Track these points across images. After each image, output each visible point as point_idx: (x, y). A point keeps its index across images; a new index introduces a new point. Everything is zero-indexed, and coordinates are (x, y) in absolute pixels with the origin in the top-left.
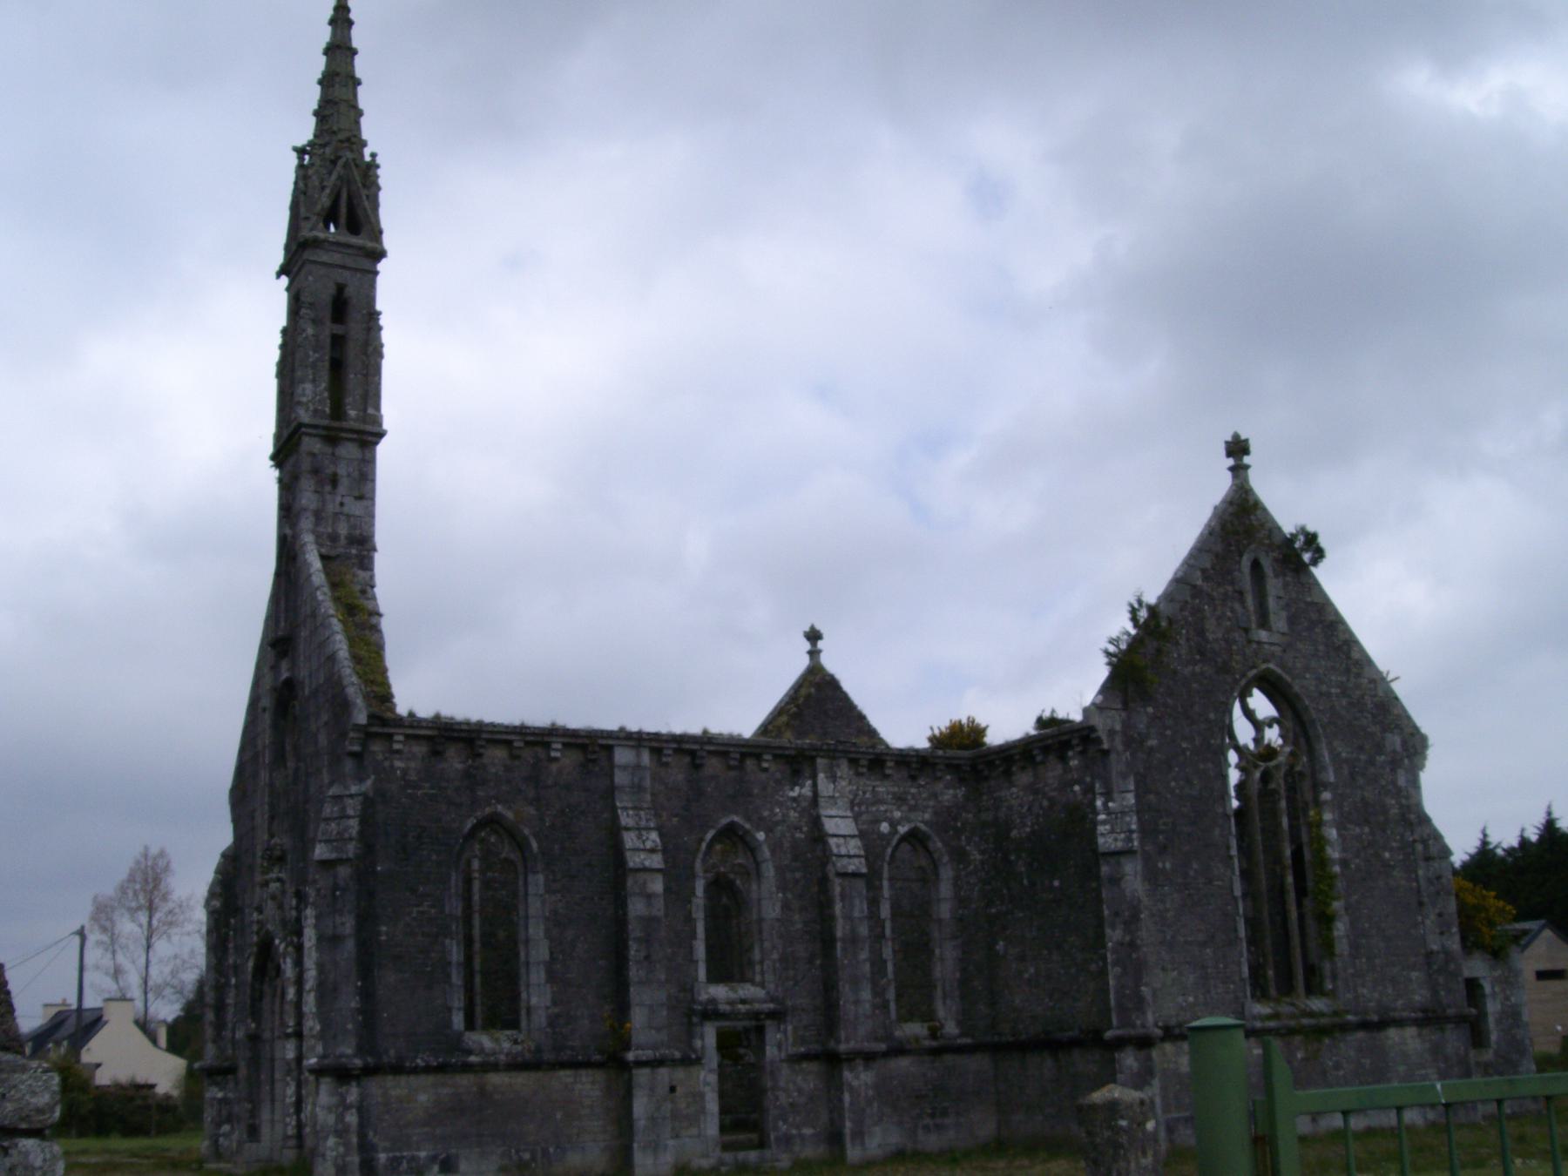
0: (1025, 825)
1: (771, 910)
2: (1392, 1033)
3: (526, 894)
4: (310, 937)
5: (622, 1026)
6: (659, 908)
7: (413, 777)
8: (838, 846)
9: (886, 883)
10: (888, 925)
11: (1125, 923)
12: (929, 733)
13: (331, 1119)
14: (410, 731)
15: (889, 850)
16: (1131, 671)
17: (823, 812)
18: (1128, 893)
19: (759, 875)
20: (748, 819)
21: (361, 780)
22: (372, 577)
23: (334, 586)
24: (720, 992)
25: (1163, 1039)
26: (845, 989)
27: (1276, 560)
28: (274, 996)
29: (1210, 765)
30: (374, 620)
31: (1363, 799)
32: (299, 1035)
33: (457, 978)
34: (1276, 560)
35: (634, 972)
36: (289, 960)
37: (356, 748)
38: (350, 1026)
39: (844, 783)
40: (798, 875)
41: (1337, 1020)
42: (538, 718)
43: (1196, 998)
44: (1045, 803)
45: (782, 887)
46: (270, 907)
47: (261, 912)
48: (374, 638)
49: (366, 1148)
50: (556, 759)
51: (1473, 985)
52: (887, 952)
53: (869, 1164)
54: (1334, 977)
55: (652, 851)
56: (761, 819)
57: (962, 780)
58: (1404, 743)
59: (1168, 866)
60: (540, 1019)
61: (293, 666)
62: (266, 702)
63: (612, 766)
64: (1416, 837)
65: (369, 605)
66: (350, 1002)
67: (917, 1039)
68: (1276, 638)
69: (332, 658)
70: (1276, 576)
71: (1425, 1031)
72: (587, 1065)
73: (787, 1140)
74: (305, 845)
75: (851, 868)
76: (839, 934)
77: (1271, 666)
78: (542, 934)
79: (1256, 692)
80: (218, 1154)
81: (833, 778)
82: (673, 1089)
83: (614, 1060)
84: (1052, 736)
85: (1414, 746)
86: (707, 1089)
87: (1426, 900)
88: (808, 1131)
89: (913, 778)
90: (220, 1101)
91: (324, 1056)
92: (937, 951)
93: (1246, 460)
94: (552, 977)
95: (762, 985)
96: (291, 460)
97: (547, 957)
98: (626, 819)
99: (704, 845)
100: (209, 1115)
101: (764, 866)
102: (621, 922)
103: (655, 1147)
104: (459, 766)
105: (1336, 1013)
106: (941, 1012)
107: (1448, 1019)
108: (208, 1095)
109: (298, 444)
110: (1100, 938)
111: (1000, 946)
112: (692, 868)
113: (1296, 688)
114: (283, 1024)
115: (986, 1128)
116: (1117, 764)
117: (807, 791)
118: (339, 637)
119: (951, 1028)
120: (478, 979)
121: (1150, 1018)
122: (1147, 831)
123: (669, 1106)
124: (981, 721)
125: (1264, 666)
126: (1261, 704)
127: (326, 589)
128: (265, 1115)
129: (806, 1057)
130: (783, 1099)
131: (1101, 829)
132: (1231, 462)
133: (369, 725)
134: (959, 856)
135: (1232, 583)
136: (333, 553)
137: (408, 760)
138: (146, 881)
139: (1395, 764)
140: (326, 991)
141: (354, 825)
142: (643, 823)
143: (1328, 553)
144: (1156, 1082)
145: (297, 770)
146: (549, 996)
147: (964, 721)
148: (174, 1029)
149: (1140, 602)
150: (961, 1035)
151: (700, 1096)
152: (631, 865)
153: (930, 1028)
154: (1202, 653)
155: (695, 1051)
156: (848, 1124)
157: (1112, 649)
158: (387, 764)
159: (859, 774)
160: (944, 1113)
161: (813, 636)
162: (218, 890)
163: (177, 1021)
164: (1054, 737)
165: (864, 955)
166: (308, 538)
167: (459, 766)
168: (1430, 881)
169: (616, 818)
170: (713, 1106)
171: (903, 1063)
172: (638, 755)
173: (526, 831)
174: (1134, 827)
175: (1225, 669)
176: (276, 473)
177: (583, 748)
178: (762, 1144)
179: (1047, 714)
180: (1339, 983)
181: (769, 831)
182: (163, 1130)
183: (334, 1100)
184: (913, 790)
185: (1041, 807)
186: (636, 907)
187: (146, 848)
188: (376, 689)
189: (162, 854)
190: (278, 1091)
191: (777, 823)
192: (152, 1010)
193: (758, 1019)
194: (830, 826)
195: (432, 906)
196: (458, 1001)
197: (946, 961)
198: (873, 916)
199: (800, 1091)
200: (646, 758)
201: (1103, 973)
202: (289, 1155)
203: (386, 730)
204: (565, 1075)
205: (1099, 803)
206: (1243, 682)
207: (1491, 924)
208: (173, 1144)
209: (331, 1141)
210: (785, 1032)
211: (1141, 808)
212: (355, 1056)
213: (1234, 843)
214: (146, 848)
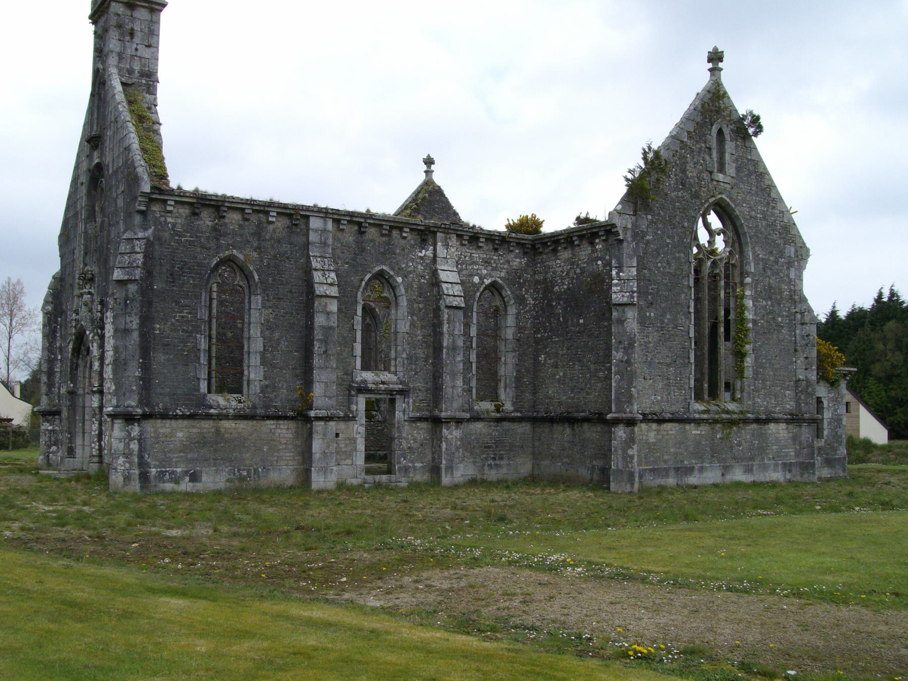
0: (564, 284)
1: (403, 327)
2: (772, 426)
3: (250, 308)
4: (109, 330)
5: (308, 394)
6: (334, 321)
7: (179, 228)
8: (448, 289)
9: (475, 314)
10: (474, 340)
11: (624, 348)
12: (507, 223)
13: (121, 446)
14: (178, 199)
15: (478, 294)
16: (639, 193)
17: (439, 267)
18: (628, 330)
19: (397, 304)
20: (393, 269)
21: (146, 229)
22: (155, 99)
23: (130, 103)
24: (369, 376)
25: (641, 421)
26: (447, 378)
27: (732, 130)
28: (85, 366)
29: (682, 255)
30: (156, 127)
31: (769, 284)
32: (101, 392)
33: (203, 360)
34: (732, 130)
35: (316, 361)
36: (95, 344)
37: (143, 208)
38: (134, 388)
39: (453, 250)
40: (421, 306)
41: (742, 416)
42: (262, 196)
43: (662, 397)
44: (578, 271)
45: (412, 313)
46: (84, 311)
47: (78, 314)
48: (156, 138)
49: (142, 464)
50: (272, 222)
51: (819, 401)
52: (473, 357)
53: (456, 487)
54: (742, 391)
55: (331, 284)
56: (400, 269)
57: (525, 253)
58: (796, 251)
59: (652, 315)
60: (256, 388)
61: (102, 155)
62: (84, 179)
63: (308, 229)
64: (797, 310)
65: (153, 117)
66: (134, 371)
67: (488, 412)
68: (728, 180)
69: (128, 149)
70: (731, 141)
71: (790, 427)
72: (285, 418)
73: (406, 470)
74: (107, 270)
75: (455, 304)
76: (445, 345)
77: (724, 196)
78: (259, 334)
79: (712, 212)
80: (49, 464)
81: (447, 246)
82: (337, 435)
83: (302, 416)
84: (586, 229)
85: (801, 254)
86: (358, 436)
87: (799, 348)
88: (418, 465)
89: (496, 250)
90: (51, 431)
91: (117, 406)
92: (503, 359)
93: (720, 65)
94: (264, 362)
95: (395, 373)
96: (103, 19)
97: (262, 349)
98: (315, 264)
99: (364, 283)
100: (43, 439)
101: (400, 298)
102: (309, 328)
103: (325, 471)
104: (210, 223)
105: (741, 412)
106: (503, 396)
107: (804, 420)
108: (42, 428)
109: (108, 7)
110: (608, 356)
111: (542, 358)
112: (356, 297)
113: (737, 212)
114: (91, 385)
115: (525, 466)
116: (628, 248)
117: (430, 253)
118: (132, 135)
119: (508, 406)
120: (214, 361)
121: (635, 407)
122: (642, 293)
123: (335, 445)
124: (540, 217)
125: (720, 196)
126: (714, 221)
127: (125, 104)
128: (79, 441)
129: (420, 419)
130: (405, 445)
131: (614, 289)
132: (710, 65)
133: (152, 193)
134: (521, 300)
135: (705, 142)
136: (130, 82)
137: (177, 217)
138: (9, 298)
139: (789, 264)
140: (119, 365)
141: (140, 257)
142: (326, 267)
143: (765, 129)
144: (635, 447)
145: (103, 222)
146: (262, 374)
147: (530, 216)
148: (24, 387)
149: (650, 148)
150: (516, 410)
151: (354, 440)
152: (318, 293)
153: (495, 406)
154: (683, 184)
155: (352, 412)
156: (444, 462)
157: (630, 176)
158: (162, 219)
159: (462, 245)
160: (501, 458)
161: (429, 162)
162: (50, 299)
163: (27, 381)
164: (587, 231)
165: (459, 358)
166: (113, 71)
167: (210, 223)
168: (802, 337)
169: (309, 262)
170: (361, 446)
171: (479, 426)
172: (325, 223)
173: (251, 268)
174: (635, 289)
175: (696, 196)
176: (92, 28)
177: (290, 216)
178: (389, 472)
179: (583, 216)
180: (745, 394)
181: (405, 277)
182: (16, 447)
183: (123, 434)
184: (495, 258)
185: (575, 273)
186: (320, 320)
187: (9, 279)
188: (156, 170)
189: (19, 282)
190: (87, 427)
191: (410, 272)
192: (12, 375)
193: (392, 395)
194: (443, 276)
195: (189, 313)
196: (203, 375)
197: (507, 367)
198: (466, 334)
199: (415, 440)
200: (330, 225)
201: (608, 378)
202: (94, 468)
203: (162, 197)
204: (270, 423)
205: (614, 273)
206: (706, 205)
207: (834, 366)
208: (22, 456)
209: (121, 460)
210: (408, 402)
211: (639, 278)
212: (137, 407)
213: (692, 304)
214: (9, 279)
